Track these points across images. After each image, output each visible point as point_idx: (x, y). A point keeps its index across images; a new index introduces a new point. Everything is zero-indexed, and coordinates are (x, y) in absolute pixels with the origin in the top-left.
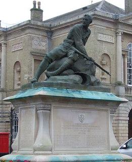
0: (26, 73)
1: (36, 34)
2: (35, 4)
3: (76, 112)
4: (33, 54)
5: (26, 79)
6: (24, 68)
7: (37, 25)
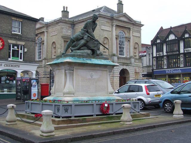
2: (64, 8)
4: (63, 37)
5: (59, 52)
6: (58, 46)
7: (66, 21)
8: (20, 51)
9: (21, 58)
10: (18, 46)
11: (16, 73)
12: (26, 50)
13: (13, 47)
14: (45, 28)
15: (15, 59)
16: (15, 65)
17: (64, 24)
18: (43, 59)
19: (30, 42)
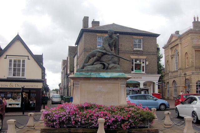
0: (190, 59)
1: (195, 36)
2: (195, 19)
3: (96, 85)
4: (193, 47)
5: (191, 62)
6: (190, 56)
7: (196, 31)
8: (142, 65)
9: (143, 71)
10: (140, 60)
11: (139, 84)
12: (147, 63)
13: (136, 61)
14: (179, 40)
15: (138, 71)
16: (137, 76)
17: (194, 34)
18: (179, 70)
19: (151, 56)
